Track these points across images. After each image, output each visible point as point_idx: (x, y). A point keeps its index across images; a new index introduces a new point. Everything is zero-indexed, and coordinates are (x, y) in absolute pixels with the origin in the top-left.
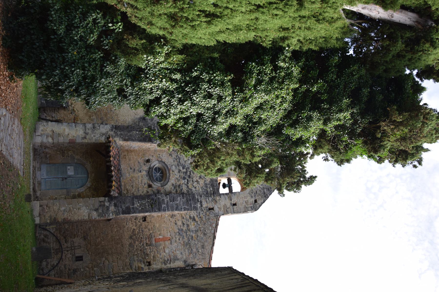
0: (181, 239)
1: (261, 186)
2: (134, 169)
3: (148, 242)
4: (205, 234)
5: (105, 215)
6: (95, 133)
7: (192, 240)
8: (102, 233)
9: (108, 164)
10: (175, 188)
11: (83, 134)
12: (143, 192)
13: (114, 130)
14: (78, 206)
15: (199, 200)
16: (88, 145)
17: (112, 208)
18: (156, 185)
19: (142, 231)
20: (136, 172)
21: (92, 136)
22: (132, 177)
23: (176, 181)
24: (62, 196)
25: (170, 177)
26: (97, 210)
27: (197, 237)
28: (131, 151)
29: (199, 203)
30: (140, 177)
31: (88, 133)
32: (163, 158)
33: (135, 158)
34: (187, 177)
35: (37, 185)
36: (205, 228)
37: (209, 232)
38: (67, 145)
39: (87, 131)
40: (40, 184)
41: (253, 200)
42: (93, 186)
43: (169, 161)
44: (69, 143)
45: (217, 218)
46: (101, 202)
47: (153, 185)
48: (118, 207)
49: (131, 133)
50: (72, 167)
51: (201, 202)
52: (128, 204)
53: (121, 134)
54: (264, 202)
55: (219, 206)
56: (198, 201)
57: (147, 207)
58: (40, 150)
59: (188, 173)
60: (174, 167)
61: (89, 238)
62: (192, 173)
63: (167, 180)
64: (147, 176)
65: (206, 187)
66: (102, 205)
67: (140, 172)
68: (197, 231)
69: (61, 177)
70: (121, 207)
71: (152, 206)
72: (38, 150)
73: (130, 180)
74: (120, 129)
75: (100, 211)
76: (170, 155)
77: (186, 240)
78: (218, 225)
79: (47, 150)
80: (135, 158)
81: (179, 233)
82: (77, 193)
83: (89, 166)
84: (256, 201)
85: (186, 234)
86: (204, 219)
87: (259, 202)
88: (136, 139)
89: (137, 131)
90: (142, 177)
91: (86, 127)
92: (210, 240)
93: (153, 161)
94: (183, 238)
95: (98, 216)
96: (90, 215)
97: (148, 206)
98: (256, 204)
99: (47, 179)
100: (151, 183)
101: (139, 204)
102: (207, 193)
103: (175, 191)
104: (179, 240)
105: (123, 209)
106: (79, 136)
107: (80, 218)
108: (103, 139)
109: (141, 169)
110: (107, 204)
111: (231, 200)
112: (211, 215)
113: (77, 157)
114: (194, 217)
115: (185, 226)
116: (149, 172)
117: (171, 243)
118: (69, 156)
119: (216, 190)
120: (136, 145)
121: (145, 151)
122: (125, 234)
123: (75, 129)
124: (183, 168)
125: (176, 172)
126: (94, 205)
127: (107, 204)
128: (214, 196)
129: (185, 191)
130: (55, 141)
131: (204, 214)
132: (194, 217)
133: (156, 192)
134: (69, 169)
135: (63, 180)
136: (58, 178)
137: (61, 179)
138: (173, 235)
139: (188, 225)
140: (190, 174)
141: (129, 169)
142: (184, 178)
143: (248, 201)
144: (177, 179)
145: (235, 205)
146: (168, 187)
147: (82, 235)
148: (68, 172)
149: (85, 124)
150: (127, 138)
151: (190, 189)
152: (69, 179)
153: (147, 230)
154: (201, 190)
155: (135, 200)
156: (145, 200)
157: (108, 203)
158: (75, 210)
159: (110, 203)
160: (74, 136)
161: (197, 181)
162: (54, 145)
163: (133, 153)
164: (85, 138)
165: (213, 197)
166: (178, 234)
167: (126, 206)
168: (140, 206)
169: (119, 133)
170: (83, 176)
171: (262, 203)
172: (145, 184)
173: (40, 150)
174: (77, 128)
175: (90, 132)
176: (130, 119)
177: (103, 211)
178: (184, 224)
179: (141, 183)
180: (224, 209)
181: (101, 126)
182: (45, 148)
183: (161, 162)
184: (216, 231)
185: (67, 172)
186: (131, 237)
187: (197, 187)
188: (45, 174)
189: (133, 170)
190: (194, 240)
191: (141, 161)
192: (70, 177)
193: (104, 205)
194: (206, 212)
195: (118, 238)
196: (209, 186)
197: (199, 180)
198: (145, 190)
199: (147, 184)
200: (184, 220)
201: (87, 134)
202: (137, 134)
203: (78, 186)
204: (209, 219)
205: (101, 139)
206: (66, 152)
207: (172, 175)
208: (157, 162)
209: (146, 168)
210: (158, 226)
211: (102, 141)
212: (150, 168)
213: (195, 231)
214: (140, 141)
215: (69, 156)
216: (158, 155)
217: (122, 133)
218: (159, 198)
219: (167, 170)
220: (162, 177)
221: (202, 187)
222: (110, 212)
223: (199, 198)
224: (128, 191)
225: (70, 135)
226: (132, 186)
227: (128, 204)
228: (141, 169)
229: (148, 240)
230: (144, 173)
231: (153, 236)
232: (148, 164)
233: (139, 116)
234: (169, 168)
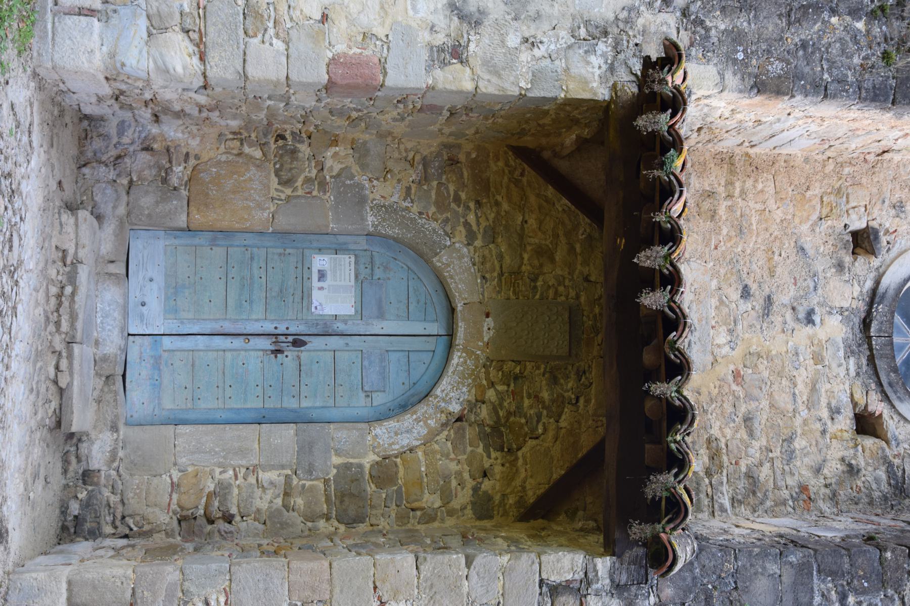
2: (769, 300)
6: (538, 17)
9: (653, 300)
11: (441, 21)
12: (818, 471)
16: (472, 105)
20: (777, 320)
22: (753, 357)
24: (266, 476)
28: (755, 167)
30: (806, 356)
33: (778, 215)
35: (83, 384)
38: (311, 103)
40: (115, 376)
42: (484, 412)
44: (330, 87)
47: (891, 424)
49: (809, 31)
50: (347, 261)
53: (736, 37)
58: (122, 128)
64: (850, 352)
67: (809, 319)
69: (269, 327)
72: (111, 128)
79: (172, 131)
82: (369, 460)
83: (459, 264)
88: (841, 81)
90: (818, 359)
99: (166, 341)
100: (877, 406)
108: (592, 77)
109: (814, 300)
113: (387, 192)
116: (866, 324)
118: (323, 185)
130: (222, 68)
136: (247, 335)
148: (318, 297)
150: (776, 67)
152: (315, 343)
160: (366, 35)
162: (212, 100)
163: (765, 183)
164: (456, 52)
170: (418, 328)
172: (834, 412)
173: (122, 128)
179: (811, 404)
182: (156, 118)
185: (305, 296)
188: (155, 306)
191: (821, 239)
198: (836, 451)
203: (379, 399)
205: (578, 68)
206: (304, 149)
211: (585, 82)
215: (323, 185)
225: (340, 28)
226: (748, 420)
228: (814, 300)
230: (835, 330)
232: (863, 266)
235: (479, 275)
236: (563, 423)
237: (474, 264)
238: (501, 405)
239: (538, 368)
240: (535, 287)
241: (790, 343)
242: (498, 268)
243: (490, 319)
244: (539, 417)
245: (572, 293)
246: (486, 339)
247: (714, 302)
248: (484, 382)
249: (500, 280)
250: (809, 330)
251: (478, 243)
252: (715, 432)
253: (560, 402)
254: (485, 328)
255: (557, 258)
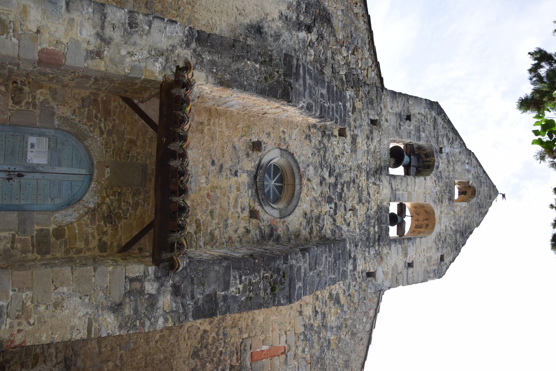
0: (307, 350)
1: (453, 228)
2: (221, 166)
3: (234, 362)
4: (353, 334)
5: (143, 325)
6: (135, 44)
7: (328, 349)
8: (120, 345)
10: (308, 223)
11: (93, 40)
12: (236, 231)
13: (193, 45)
14: (53, 296)
15: (352, 256)
16: (102, 79)
17: (166, 301)
18: (269, 214)
19: (225, 334)
20: (224, 174)
21: (123, 52)
22: (214, 188)
23: (314, 204)
25: (302, 195)
26: (116, 308)
27: (339, 342)
28: (219, 114)
29: (351, 261)
31: (111, 39)
32: (291, 143)
33: (227, 133)
34: (335, 198)
36: (354, 320)
37: (361, 327)
39: (108, 32)
41: (439, 255)
42: (104, 207)
43: (304, 152)
44: (40, 62)
45: (379, 293)
46: (132, 280)
47: (262, 214)
48: (183, 297)
49: (240, 65)
50: (45, 141)
51: (355, 259)
52: (213, 287)
53: (213, 63)
54: (453, 261)
55: (386, 269)
56: (350, 257)
57: (262, 294)
59: (339, 187)
60: (311, 168)
61: (79, 363)
62: (345, 189)
63: (294, 202)
64: (249, 187)
65: (368, 224)
66: (135, 290)
67: (236, 174)
68: (339, 328)
69: (6, 168)
70: (193, 297)
71: (273, 289)
73: (208, 195)
74: (212, 46)
75: (128, 311)
76: (306, 138)
77: (316, 351)
78: (379, 312)
80: (227, 133)
81: (305, 336)
82: (52, 227)
83: (96, 143)
84: (442, 258)
85: (319, 337)
86: (356, 300)
87: (446, 260)
88: (250, 85)
89: (256, 61)
90: (238, 189)
91: (104, 16)
92: (362, 348)
93: (269, 147)
94: (312, 347)
95: (120, 327)
96: (95, 325)
97: (265, 290)
98: (443, 263)
100: (258, 208)
101: (241, 287)
102: (368, 239)
103: (308, 229)
104: (304, 351)
105: (196, 303)
106: (76, 43)
107: (57, 338)
109: (238, 167)
110: (150, 288)
111: (406, 255)
112: (369, 291)
114: (338, 294)
115: (319, 316)
116: (255, 177)
117: (286, 362)
118: (34, 106)
119: (384, 232)
120: (238, 100)
121: (251, 119)
122: (183, 345)
123: (67, 16)
124: (330, 176)
125: (316, 181)
126: (107, 291)
127: (150, 288)
128: (379, 245)
129: (329, 231)
131: (357, 288)
132: (338, 294)
133: (267, 231)
134: (32, 146)
135: (9, 179)
137: (4, 175)
138: (292, 339)
139: (324, 315)
140: (342, 189)
141: (209, 163)
142: (330, 200)
143: (431, 257)
144: (315, 199)
145: (410, 265)
146: (295, 220)
147: (61, 356)
148: (30, 155)
149: (103, 5)
150: (228, 77)
151: (338, 227)
152: (28, 176)
153: (236, 331)
154: (358, 230)
155: (234, 273)
156: (259, 272)
157: (156, 285)
158: (42, 308)
159: (162, 285)
161: (353, 209)
163: (223, 121)
164: (99, 54)
165: (377, 248)
166: (302, 337)
167: (207, 292)
168: (244, 291)
169: (207, 57)
170: (76, 171)
171: (451, 263)
174: (75, 15)
175: (117, 36)
176: (224, 25)
177: (136, 311)
178: (317, 312)
179: (235, 206)
180: (392, 274)
181: (157, 24)
183: (286, 152)
184: (373, 326)
185: (25, 154)
186: (195, 354)
187: (352, 224)
189: (217, 167)
190: (333, 350)
191: (241, 144)
192: (34, 169)
193: (141, 291)
194: (360, 283)
195: (162, 357)
196: (373, 221)
197: (357, 207)
199: (247, 210)
200: (317, 303)
201: (106, 41)
202: (256, 69)
203: (58, 201)
204: (365, 299)
207: (305, 190)
208: (277, 152)
209: (249, 165)
210: (261, 320)
211: (153, 73)
212: (259, 167)
213: (337, 327)
214: (262, 93)
216: (282, 135)
217: (216, 58)
218: (291, 267)
219: (297, 175)
220: (280, 189)
221: (360, 224)
222: (160, 312)
223: (353, 249)
224: (198, 226)
226: (211, 212)
227: (213, 287)
228: (238, 167)
229: (235, 358)
230: (244, 178)
231: (248, 348)
232: (255, 155)
233: (247, 21)
234: (302, 170)
235: (104, 149)
236: (138, 213)
237: (102, 145)
238: (112, 205)
239: (128, 190)
240: (128, 156)
241: (308, 311)
242: (113, 147)
243: (108, 169)
244: (128, 210)
245: (144, 159)
246: (106, 177)
247: (201, 166)
248: (105, 195)
249: (113, 152)
250: (235, 178)
251: (105, 136)
252: (199, 217)
253: (137, 204)
254: (106, 172)
255: (138, 145)
